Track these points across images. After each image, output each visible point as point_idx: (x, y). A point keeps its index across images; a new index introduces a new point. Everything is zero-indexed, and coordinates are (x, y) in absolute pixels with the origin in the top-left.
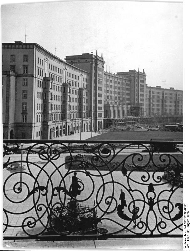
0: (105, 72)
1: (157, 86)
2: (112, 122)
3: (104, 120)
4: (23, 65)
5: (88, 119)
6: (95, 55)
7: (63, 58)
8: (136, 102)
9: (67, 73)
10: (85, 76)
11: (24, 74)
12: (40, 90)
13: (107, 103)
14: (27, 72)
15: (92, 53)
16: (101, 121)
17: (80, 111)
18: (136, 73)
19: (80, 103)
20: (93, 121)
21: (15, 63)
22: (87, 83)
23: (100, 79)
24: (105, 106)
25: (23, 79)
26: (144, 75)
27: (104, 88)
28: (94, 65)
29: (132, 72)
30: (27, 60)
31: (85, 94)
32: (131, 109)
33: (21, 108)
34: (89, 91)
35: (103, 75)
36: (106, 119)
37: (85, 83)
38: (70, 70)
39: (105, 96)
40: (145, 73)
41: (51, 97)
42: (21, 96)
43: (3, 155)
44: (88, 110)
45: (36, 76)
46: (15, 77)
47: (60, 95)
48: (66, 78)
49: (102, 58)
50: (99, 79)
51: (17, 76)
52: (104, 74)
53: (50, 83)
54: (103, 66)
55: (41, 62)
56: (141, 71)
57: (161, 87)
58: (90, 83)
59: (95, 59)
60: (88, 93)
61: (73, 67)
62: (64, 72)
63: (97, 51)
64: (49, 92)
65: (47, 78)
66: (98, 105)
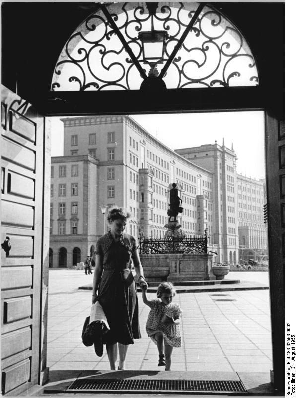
0: (239, 175)
2: (252, 254)
3: (240, 251)
4: (108, 148)
5: (212, 246)
6: (222, 145)
9: (176, 169)
10: (205, 177)
11: (109, 161)
12: (135, 187)
13: (243, 224)
14: (113, 158)
15: (216, 142)
16: (235, 252)
17: (200, 220)
19: (199, 218)
20: (220, 250)
21: (97, 146)
22: (209, 190)
23: (230, 184)
24: (240, 230)
25: (108, 168)
27: (238, 210)
28: (219, 161)
30: (113, 140)
31: (206, 205)
33: (106, 175)
34: (212, 202)
35: (236, 179)
36: (243, 249)
37: (206, 188)
38: (180, 165)
39: (240, 214)
41: (152, 216)
42: (106, 195)
44: (212, 232)
45: (128, 164)
46: (96, 166)
47: (166, 202)
49: (233, 151)
50: (228, 183)
51: (99, 165)
52: (238, 178)
53: (150, 178)
54: (234, 164)
55: (133, 142)
61: (185, 160)
62: (171, 167)
63: (223, 139)
64: (148, 190)
65: (144, 169)
66: (229, 225)
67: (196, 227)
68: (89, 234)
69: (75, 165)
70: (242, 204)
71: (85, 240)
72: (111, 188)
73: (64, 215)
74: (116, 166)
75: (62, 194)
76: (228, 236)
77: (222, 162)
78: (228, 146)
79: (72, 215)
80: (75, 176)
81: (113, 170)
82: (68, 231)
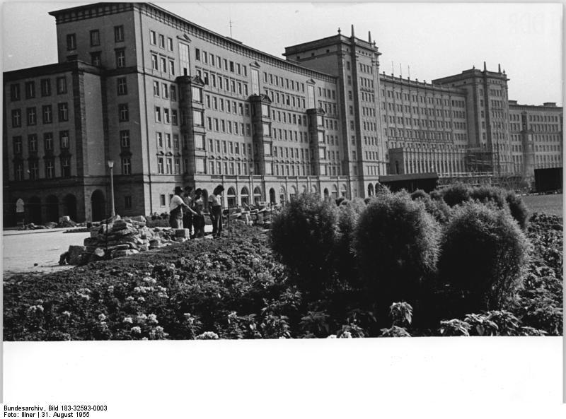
1: (546, 102)
7: (279, 53)
8: (483, 141)
11: (118, 68)
15: (339, 31)
17: (313, 161)
18: (476, 73)
20: (352, 183)
26: (501, 78)
29: (470, 75)
32: (468, 158)
34: (338, 118)
37: (323, 99)
40: (506, 73)
43: (522, 337)
44: (338, 158)
47: (242, 122)
48: (317, 100)
54: (373, 62)
56: (492, 68)
57: (557, 105)
58: (339, 100)
59: (347, 45)
60: (336, 122)
64: (192, 107)
67: (307, 155)
68: (144, 173)
69: (62, 78)
70: (402, 118)
71: (79, 184)
72: (123, 107)
73: (129, 147)
74: (128, 76)
75: (33, 123)
76: (364, 164)
77: (352, 61)
78: (361, 35)
79: (61, 149)
80: (63, 93)
81: (125, 81)
82: (58, 173)
